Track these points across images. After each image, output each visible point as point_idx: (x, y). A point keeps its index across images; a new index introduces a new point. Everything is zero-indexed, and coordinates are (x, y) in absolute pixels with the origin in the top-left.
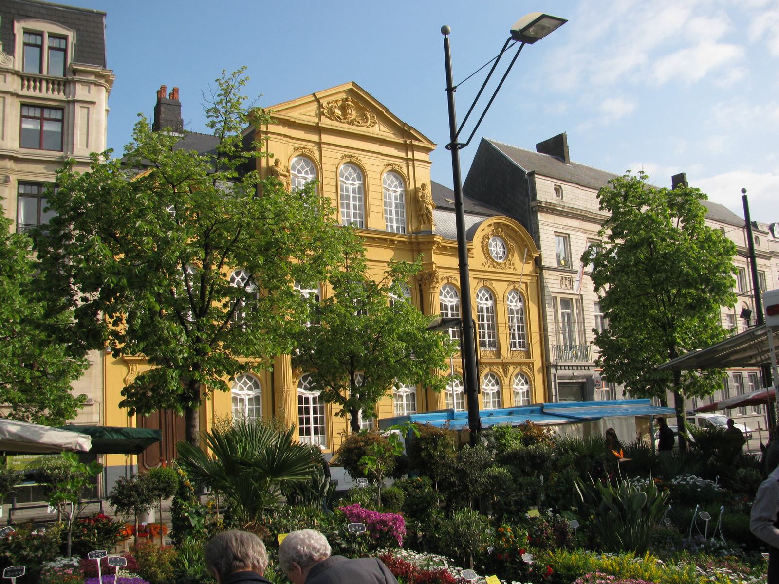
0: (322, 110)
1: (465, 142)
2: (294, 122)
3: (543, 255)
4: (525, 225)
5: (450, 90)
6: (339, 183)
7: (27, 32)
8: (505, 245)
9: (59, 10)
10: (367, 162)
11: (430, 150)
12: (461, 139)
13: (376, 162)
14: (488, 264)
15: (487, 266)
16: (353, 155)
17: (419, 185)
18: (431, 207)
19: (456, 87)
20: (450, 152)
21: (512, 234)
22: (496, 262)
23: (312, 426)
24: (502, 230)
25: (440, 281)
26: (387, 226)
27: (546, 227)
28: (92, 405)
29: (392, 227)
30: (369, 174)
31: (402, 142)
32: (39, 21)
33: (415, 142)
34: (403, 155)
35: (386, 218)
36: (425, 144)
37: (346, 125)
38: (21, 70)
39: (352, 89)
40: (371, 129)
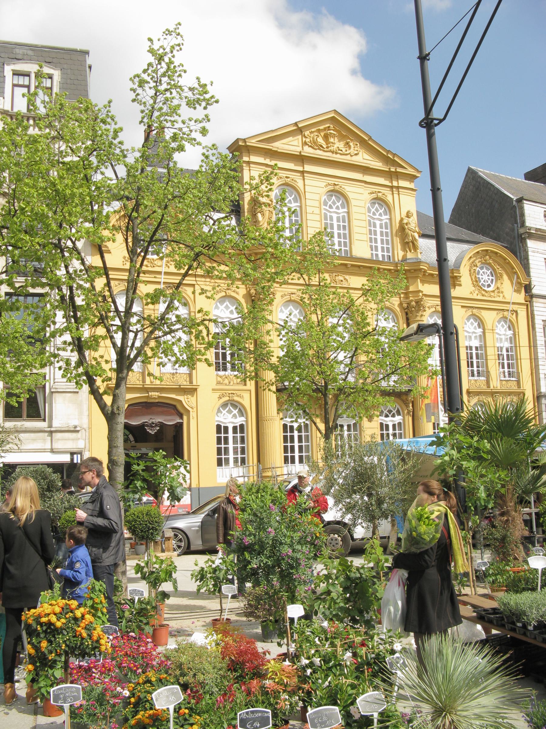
0: (304, 139)
1: (442, 117)
2: (276, 151)
3: (533, 283)
4: (514, 253)
5: (423, 58)
6: (323, 211)
7: (16, 73)
8: (494, 273)
9: (46, 51)
10: (349, 189)
11: (415, 177)
12: (437, 112)
13: (361, 190)
14: (477, 292)
15: (475, 295)
16: (336, 183)
17: (404, 214)
18: (416, 235)
19: (429, 54)
20: (425, 130)
21: (501, 261)
22: (484, 290)
23: (297, 454)
24: (490, 258)
25: (427, 309)
26: (372, 254)
27: (536, 254)
28: (78, 431)
29: (377, 255)
30: (353, 202)
31: (387, 170)
32: (26, 63)
33: (399, 170)
34: (387, 183)
35: (371, 247)
36: (410, 171)
37: (329, 154)
38: (10, 109)
39: (333, 117)
40: (355, 158)
